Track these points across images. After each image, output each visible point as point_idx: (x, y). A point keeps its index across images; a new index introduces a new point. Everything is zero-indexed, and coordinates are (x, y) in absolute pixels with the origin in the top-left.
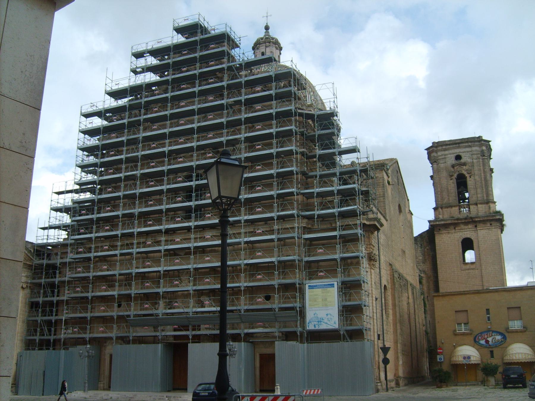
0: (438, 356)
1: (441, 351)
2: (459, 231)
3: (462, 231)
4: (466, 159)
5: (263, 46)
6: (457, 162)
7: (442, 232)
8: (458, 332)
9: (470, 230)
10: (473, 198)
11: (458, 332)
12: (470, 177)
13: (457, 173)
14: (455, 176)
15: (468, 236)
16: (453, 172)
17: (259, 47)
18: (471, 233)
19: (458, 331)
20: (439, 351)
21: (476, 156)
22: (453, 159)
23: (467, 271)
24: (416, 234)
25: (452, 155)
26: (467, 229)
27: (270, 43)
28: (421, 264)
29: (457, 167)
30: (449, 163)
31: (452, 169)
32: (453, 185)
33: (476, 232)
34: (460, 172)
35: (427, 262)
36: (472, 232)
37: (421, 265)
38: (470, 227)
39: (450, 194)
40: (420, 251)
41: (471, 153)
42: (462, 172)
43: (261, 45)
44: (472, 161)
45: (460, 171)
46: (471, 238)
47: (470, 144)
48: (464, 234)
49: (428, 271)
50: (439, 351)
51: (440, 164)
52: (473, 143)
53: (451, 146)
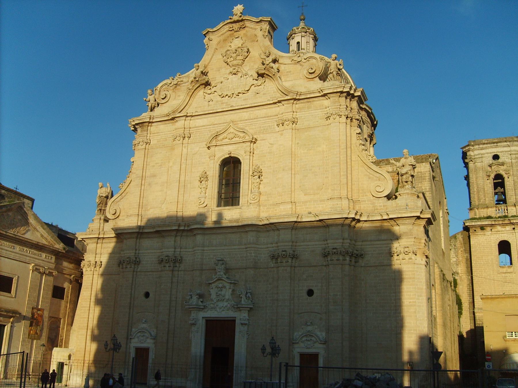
0: (486, 363)
1: (490, 358)
2: (496, 233)
3: (499, 233)
4: (504, 158)
5: (299, 36)
6: (494, 161)
7: (478, 233)
8: (508, 338)
9: (508, 232)
10: (511, 199)
11: (507, 337)
12: (508, 178)
13: (495, 173)
14: (493, 176)
15: (506, 239)
16: (490, 172)
17: (294, 36)
18: (509, 236)
19: (508, 336)
20: (487, 357)
21: (514, 156)
22: (491, 158)
23: (503, 275)
24: (450, 236)
25: (489, 154)
26: (504, 231)
27: (306, 32)
28: (455, 266)
29: (495, 167)
30: (485, 162)
31: (489, 169)
32: (490, 185)
33: (513, 235)
34: (498, 173)
35: (460, 264)
36: (509, 235)
37: (455, 267)
38: (507, 230)
39: (486, 195)
40: (454, 252)
41: (510, 153)
42: (499, 173)
43: (296, 35)
44: (510, 161)
45: (498, 171)
46: (508, 240)
47: (508, 143)
48: (501, 236)
49: (462, 273)
50: (487, 357)
51: (476, 163)
52: (512, 143)
53: (489, 145)
